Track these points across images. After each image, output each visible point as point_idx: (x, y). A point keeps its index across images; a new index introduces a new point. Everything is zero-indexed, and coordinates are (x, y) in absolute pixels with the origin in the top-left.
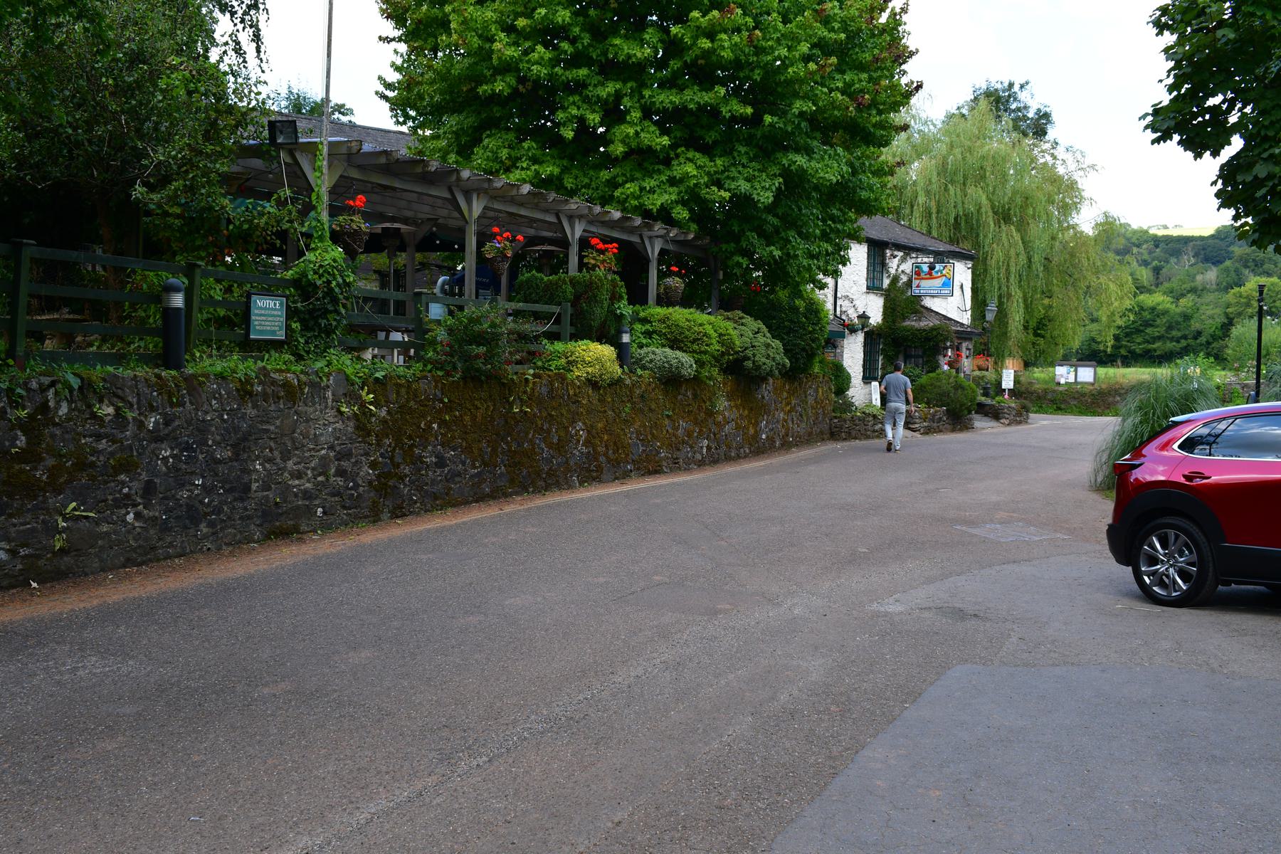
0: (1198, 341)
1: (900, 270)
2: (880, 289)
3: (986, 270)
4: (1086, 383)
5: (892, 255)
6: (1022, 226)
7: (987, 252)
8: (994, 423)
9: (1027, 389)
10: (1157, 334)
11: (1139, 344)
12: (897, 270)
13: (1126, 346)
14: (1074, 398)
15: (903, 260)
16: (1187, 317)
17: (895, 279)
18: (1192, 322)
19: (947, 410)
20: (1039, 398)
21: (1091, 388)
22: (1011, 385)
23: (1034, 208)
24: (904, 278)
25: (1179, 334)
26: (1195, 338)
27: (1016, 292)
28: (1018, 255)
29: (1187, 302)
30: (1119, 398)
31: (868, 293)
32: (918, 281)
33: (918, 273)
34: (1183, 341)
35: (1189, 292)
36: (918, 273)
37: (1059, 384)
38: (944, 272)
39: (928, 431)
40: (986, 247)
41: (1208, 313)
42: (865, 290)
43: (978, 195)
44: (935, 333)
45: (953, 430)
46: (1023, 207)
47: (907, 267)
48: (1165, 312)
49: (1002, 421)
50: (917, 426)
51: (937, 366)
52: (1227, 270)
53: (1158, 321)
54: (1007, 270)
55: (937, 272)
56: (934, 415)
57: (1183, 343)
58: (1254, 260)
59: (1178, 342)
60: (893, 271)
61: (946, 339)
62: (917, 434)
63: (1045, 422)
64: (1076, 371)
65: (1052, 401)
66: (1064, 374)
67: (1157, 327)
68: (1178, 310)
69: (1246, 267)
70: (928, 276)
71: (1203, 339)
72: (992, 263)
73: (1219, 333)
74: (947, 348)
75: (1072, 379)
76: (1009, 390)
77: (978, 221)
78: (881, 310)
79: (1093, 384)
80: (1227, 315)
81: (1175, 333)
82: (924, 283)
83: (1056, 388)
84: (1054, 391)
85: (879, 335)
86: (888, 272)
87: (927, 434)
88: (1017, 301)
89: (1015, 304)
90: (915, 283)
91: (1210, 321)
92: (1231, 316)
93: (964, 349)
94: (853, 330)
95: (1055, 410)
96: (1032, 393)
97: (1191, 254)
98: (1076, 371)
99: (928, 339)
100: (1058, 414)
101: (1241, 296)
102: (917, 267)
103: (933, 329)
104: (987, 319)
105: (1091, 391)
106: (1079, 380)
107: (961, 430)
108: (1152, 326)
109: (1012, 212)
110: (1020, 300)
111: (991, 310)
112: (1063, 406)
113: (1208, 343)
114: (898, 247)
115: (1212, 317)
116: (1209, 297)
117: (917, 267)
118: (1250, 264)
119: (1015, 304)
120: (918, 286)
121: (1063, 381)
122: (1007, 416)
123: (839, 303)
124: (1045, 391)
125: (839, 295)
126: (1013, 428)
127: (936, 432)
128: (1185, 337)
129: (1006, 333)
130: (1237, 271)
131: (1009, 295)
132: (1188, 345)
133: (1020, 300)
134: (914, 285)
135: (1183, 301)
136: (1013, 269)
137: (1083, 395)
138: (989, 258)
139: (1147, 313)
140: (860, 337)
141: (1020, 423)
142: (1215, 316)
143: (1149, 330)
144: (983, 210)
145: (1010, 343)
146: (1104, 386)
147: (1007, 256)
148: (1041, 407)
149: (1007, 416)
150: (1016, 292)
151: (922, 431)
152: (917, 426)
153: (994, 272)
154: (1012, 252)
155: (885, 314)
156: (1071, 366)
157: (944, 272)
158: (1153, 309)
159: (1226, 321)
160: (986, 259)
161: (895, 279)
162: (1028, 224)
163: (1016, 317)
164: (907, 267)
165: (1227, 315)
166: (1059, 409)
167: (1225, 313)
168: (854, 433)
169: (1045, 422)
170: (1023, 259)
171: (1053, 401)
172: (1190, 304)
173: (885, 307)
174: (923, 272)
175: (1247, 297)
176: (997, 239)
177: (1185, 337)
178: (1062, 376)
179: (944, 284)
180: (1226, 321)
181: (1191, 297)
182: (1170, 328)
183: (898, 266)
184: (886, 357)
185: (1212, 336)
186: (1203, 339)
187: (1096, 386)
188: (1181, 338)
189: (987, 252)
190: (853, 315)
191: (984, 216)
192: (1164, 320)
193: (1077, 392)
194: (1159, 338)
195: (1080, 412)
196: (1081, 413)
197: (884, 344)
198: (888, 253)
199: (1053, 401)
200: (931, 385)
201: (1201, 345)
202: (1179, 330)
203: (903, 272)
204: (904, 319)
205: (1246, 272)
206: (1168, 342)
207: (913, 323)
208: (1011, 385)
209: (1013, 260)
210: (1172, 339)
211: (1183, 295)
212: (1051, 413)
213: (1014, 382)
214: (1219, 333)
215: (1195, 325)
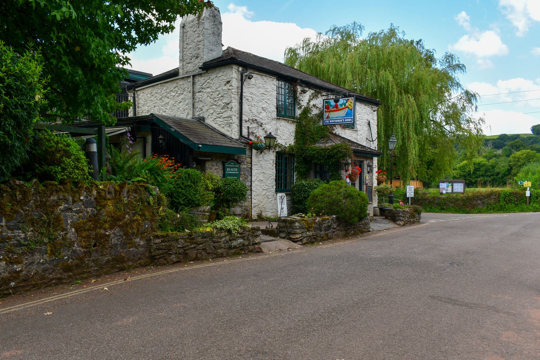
0: (498, 177)
1: (312, 103)
2: (294, 118)
3: (393, 123)
4: (459, 193)
5: (302, 91)
6: (416, 95)
7: (394, 111)
8: (391, 225)
9: (422, 197)
10: (481, 174)
11: (474, 178)
12: (308, 104)
13: (468, 179)
14: (451, 202)
15: (314, 96)
16: (493, 167)
17: (307, 111)
18: (495, 169)
19: (337, 218)
20: (430, 202)
21: (462, 195)
22: (412, 195)
23: (423, 86)
24: (315, 112)
25: (490, 174)
26: (497, 175)
27: (413, 136)
28: (413, 112)
29: (493, 161)
30: (479, 202)
31: (279, 119)
32: (327, 114)
33: (327, 107)
34: (492, 177)
35: (493, 157)
36: (327, 107)
37: (442, 193)
38: (347, 104)
39: (313, 241)
40: (393, 107)
41: (503, 165)
42: (274, 115)
43: (387, 76)
44: (335, 151)
45: (346, 236)
46: (417, 86)
47: (319, 102)
48: (484, 165)
49: (398, 223)
50: (297, 236)
51: (340, 178)
52: (506, 150)
53: (481, 169)
54: (407, 122)
55: (341, 105)
56: (320, 224)
57: (492, 177)
58: (516, 146)
59: (490, 177)
60: (304, 103)
61: (344, 156)
62: (297, 246)
63: (433, 221)
64: (452, 186)
65: (438, 204)
66: (445, 188)
67: (481, 171)
68: (490, 164)
69: (513, 148)
70: (335, 109)
71: (500, 176)
72: (397, 118)
73: (507, 173)
74: (347, 164)
75: (450, 190)
76: (411, 198)
77: (387, 91)
78: (294, 135)
79: (463, 193)
80: (509, 165)
81: (488, 173)
82: (333, 115)
83: (441, 196)
84: (439, 198)
85: (291, 155)
86: (299, 104)
87: (312, 243)
88: (414, 141)
89: (412, 143)
90: (326, 115)
91: (503, 168)
92: (512, 166)
93: (366, 166)
94: (260, 149)
95: (440, 210)
96: (426, 200)
97: (491, 144)
98: (452, 186)
99: (330, 157)
100: (442, 213)
101: (515, 158)
102: (327, 102)
103: (334, 148)
104: (390, 148)
105: (462, 197)
106: (454, 191)
107: (355, 235)
108: (479, 171)
109: (409, 87)
110: (416, 141)
111: (393, 142)
112: (445, 207)
113: (502, 177)
114: (310, 85)
115: (503, 167)
116: (502, 159)
117: (327, 102)
118: (515, 147)
119: (412, 143)
120: (328, 118)
121: (444, 192)
122: (401, 218)
123: (245, 125)
124: (434, 198)
125: (244, 118)
126: (408, 228)
127: (321, 241)
128: (493, 175)
129: (407, 162)
130: (509, 150)
131: (409, 138)
132: (494, 178)
133: (416, 141)
134: (325, 117)
135: (491, 161)
136: (411, 121)
137: (457, 200)
138: (395, 114)
139: (476, 165)
140: (270, 157)
141: (414, 223)
142: (505, 166)
143: (478, 173)
144: (390, 85)
145: (410, 168)
146: (470, 194)
147: (407, 114)
148: (432, 208)
149: (401, 218)
150: (413, 136)
151: (467, 182)
152: (297, 236)
153: (398, 123)
154: (410, 111)
155: (296, 138)
156: (449, 182)
157: (347, 104)
158: (479, 164)
159: (509, 168)
160: (393, 115)
161: (307, 111)
162: (420, 95)
163: (413, 151)
164: (319, 102)
165: (509, 165)
166: (442, 209)
167: (509, 165)
168: (193, 253)
169: (433, 221)
170: (417, 114)
171: (438, 204)
172: (494, 161)
173: (297, 132)
174: (331, 106)
175: (518, 158)
176: (400, 103)
177: (493, 175)
178: (444, 189)
179: (347, 114)
180: (509, 168)
181: (494, 159)
182: (486, 171)
183: (309, 101)
184: (299, 172)
185: (504, 174)
186: (500, 176)
187: (465, 195)
188: (491, 175)
189: (394, 111)
190: (261, 134)
191: (391, 88)
192: (484, 168)
193: (454, 198)
194: (482, 176)
195: (455, 211)
196: (456, 212)
197: (3, 104)
198: (299, 89)
199: (438, 204)
200: (322, 195)
201: (499, 178)
202: (490, 172)
203: (314, 106)
204: (315, 142)
205: (513, 150)
206: (485, 177)
207: (321, 145)
208: (412, 195)
209: (410, 115)
210: (487, 176)
211: (491, 158)
212: (437, 212)
213: (414, 193)
214: (507, 173)
215: (497, 170)
